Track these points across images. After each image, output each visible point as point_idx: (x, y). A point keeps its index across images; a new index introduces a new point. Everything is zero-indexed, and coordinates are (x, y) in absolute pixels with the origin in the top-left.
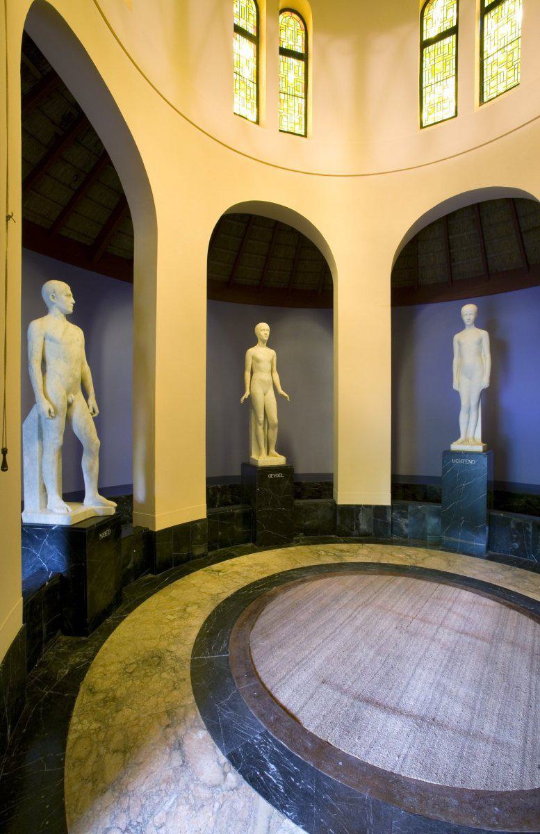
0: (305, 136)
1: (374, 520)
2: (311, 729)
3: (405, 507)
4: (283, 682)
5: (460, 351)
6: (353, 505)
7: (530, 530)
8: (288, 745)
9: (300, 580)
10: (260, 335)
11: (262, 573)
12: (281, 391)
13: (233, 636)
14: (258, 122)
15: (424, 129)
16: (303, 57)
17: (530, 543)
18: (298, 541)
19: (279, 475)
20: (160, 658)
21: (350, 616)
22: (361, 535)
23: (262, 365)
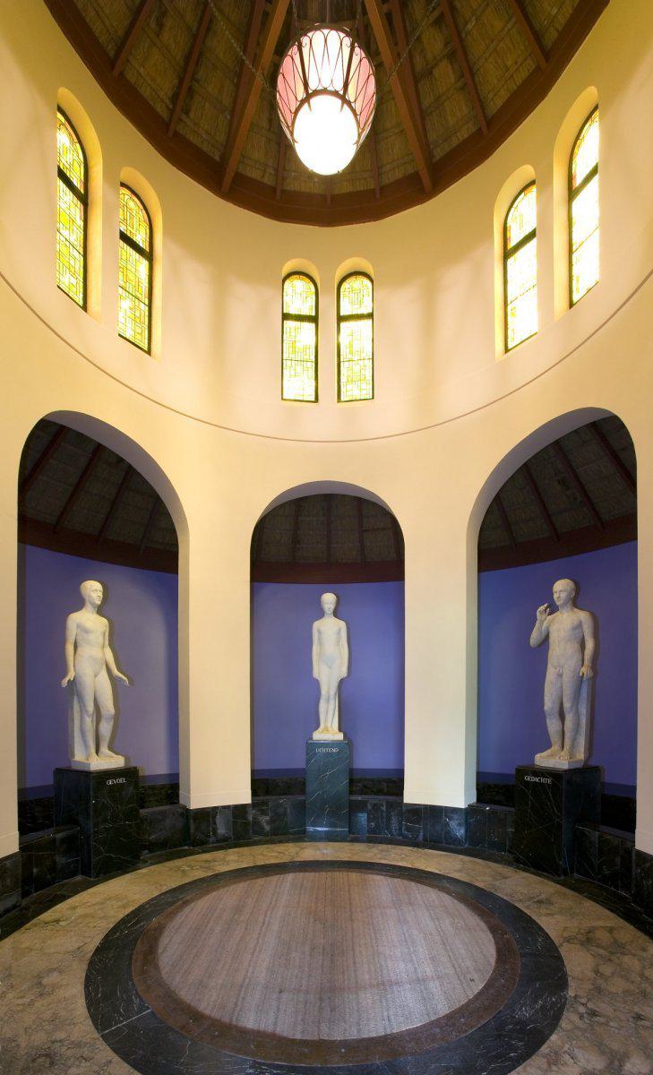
1: (234, 822)
2: (298, 1037)
3: (265, 803)
8: (285, 1062)
10: (89, 596)
11: (124, 907)
12: (116, 672)
14: (85, 308)
17: (384, 820)
19: (121, 780)
20: (47, 1055)
21: (264, 923)
22: (218, 841)
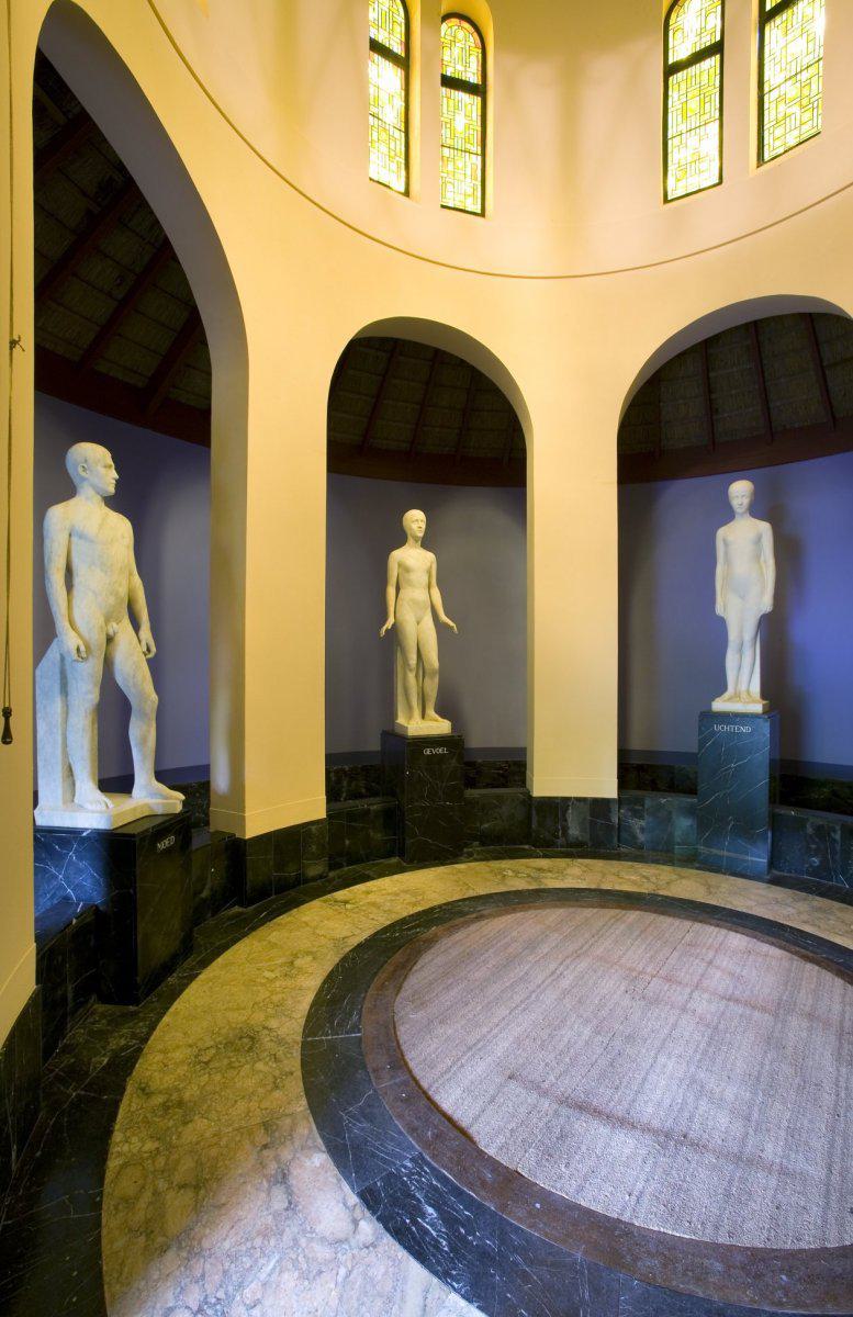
0: (483, 214)
1: (591, 821)
2: (491, 1151)
3: (640, 801)
4: (447, 1076)
5: (726, 553)
6: (557, 798)
7: (838, 837)
8: (454, 1176)
9: (474, 915)
10: (411, 529)
11: (414, 905)
12: (444, 618)
13: (367, 1004)
14: (407, 193)
15: (670, 204)
16: (478, 90)
17: (837, 857)
18: (470, 855)
19: (440, 751)
20: (252, 1038)
21: (553, 973)
22: (570, 845)
23: (413, 577)
